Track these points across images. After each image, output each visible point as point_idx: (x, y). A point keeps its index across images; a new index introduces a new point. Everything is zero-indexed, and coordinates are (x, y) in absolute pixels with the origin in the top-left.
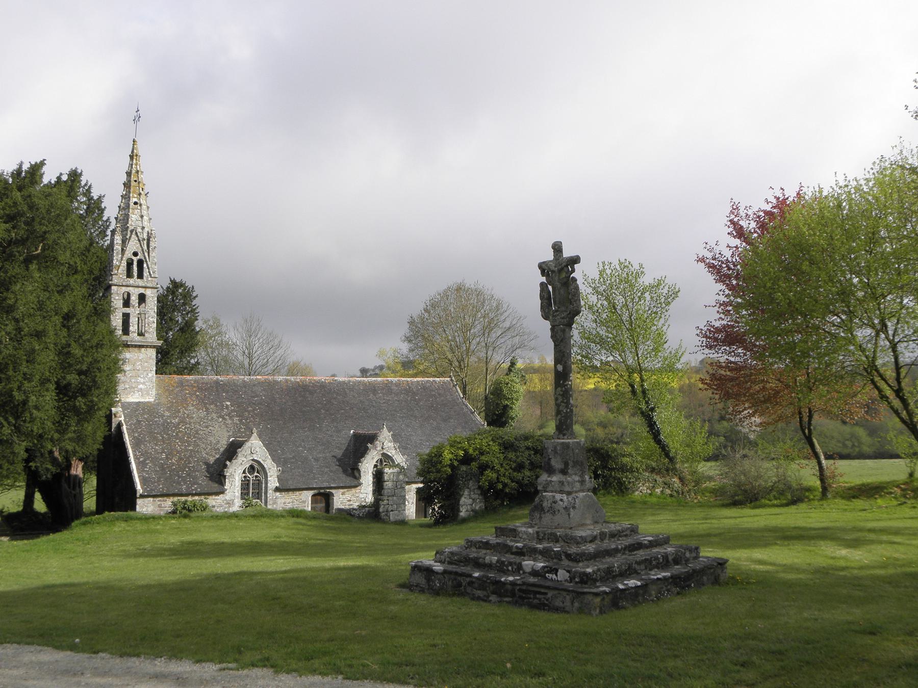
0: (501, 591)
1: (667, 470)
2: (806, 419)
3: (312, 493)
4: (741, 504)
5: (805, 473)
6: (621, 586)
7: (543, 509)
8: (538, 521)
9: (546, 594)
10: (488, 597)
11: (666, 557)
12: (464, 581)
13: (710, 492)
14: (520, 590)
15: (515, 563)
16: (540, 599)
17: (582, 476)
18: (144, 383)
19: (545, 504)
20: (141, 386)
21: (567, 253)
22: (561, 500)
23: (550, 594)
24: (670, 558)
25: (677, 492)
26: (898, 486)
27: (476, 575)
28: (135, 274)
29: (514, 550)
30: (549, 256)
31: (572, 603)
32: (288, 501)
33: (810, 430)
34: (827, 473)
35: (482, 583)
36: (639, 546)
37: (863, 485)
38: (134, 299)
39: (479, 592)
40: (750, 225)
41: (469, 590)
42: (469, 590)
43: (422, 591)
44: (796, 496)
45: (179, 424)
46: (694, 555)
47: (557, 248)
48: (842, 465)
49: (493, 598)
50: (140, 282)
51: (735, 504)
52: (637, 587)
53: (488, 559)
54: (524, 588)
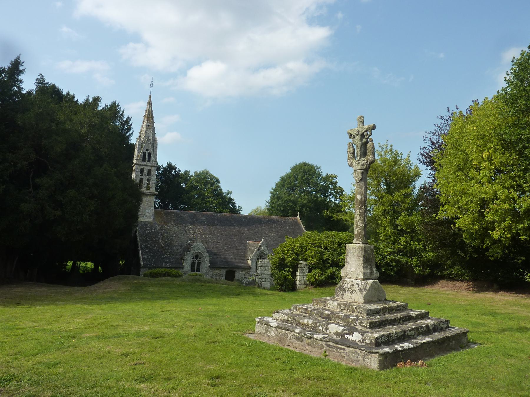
1: (326, 249)
3: (226, 270)
6: (399, 349)
7: (344, 290)
9: (345, 350)
11: (427, 326)
17: (371, 269)
18: (148, 213)
19: (346, 286)
20: (147, 214)
22: (357, 284)
24: (431, 328)
28: (147, 160)
32: (214, 273)
36: (409, 318)
38: (145, 171)
45: (164, 233)
46: (445, 326)
50: (149, 164)
52: (410, 349)
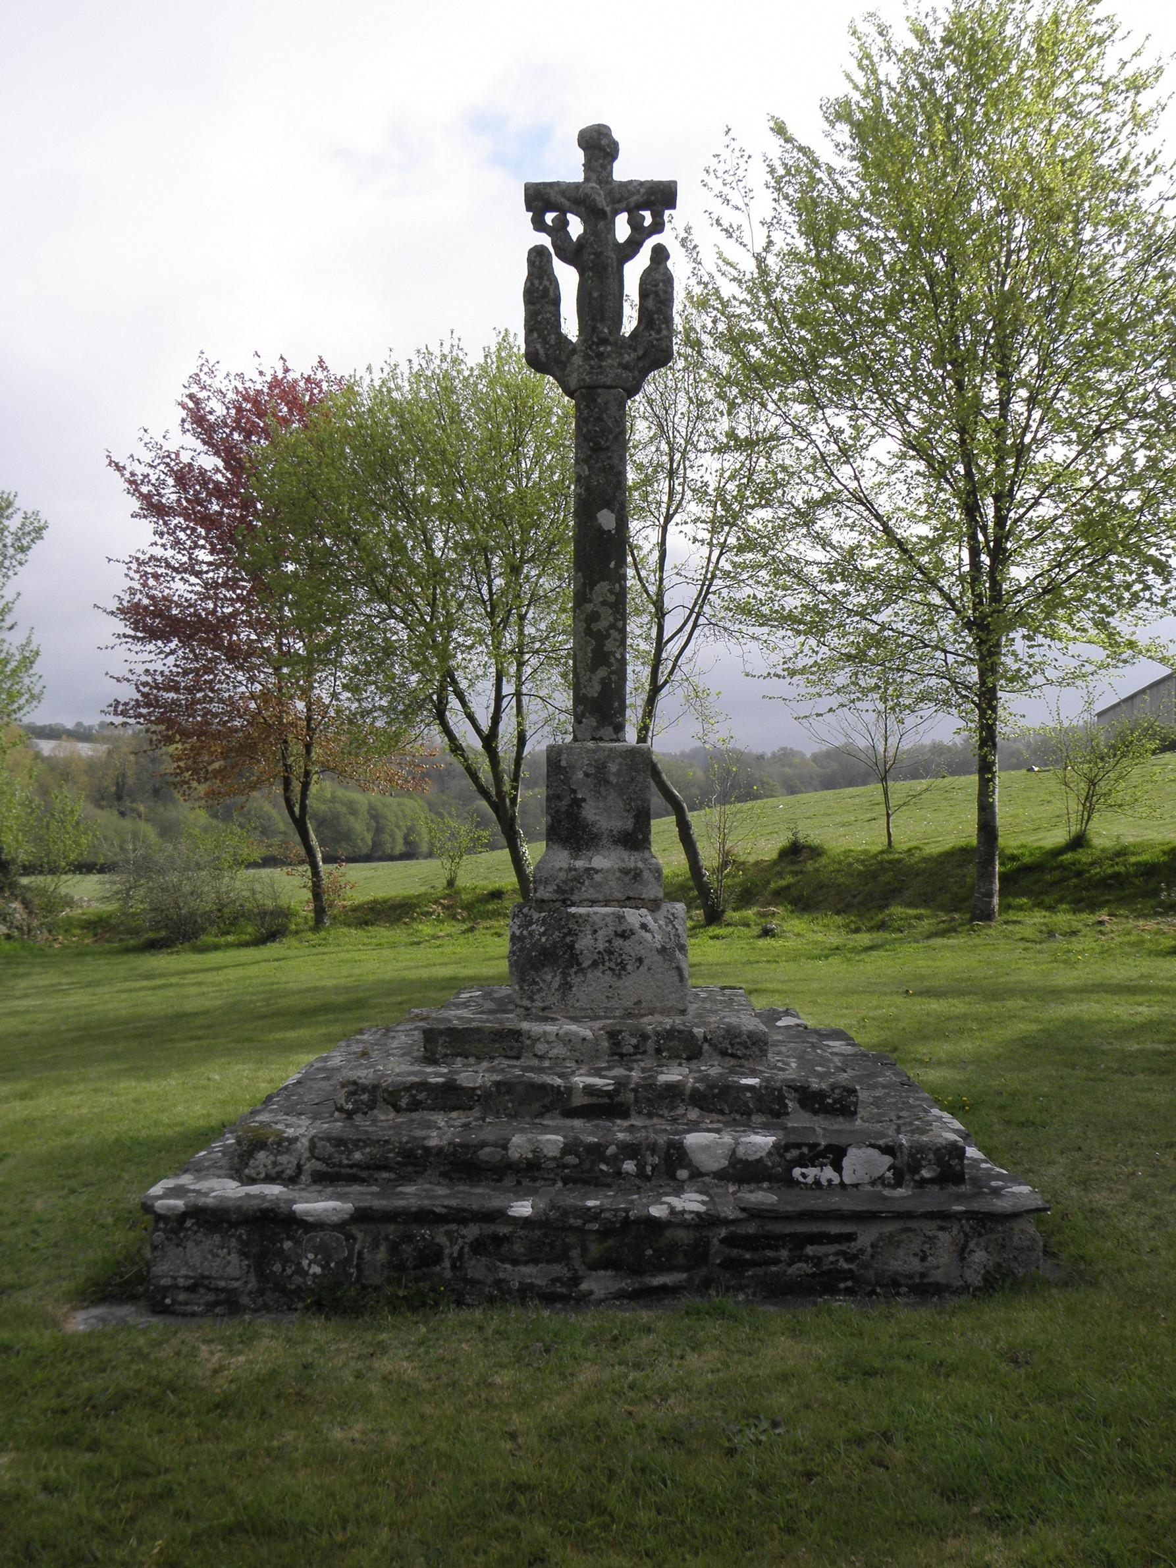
0: (647, 1261)
2: (296, 786)
4: (168, 947)
5: (289, 887)
7: (574, 959)
8: (554, 1000)
9: (850, 1237)
10: (575, 1280)
12: (451, 1242)
13: (82, 928)
14: (731, 1241)
15: (653, 1148)
16: (818, 1261)
19: (584, 943)
21: (627, 169)
23: (866, 1237)
25: (19, 929)
26: (436, 902)
27: (523, 1208)
29: (578, 1100)
30: (569, 167)
31: (962, 1254)
33: (303, 807)
34: (325, 882)
35: (547, 1238)
37: (375, 901)
39: (526, 1270)
40: (217, 409)
41: (477, 1268)
42: (477, 1268)
43: (228, 1304)
44: (271, 927)
47: (599, 146)
48: (355, 872)
49: (597, 1284)
51: (153, 946)
53: (520, 1144)
54: (751, 1229)
